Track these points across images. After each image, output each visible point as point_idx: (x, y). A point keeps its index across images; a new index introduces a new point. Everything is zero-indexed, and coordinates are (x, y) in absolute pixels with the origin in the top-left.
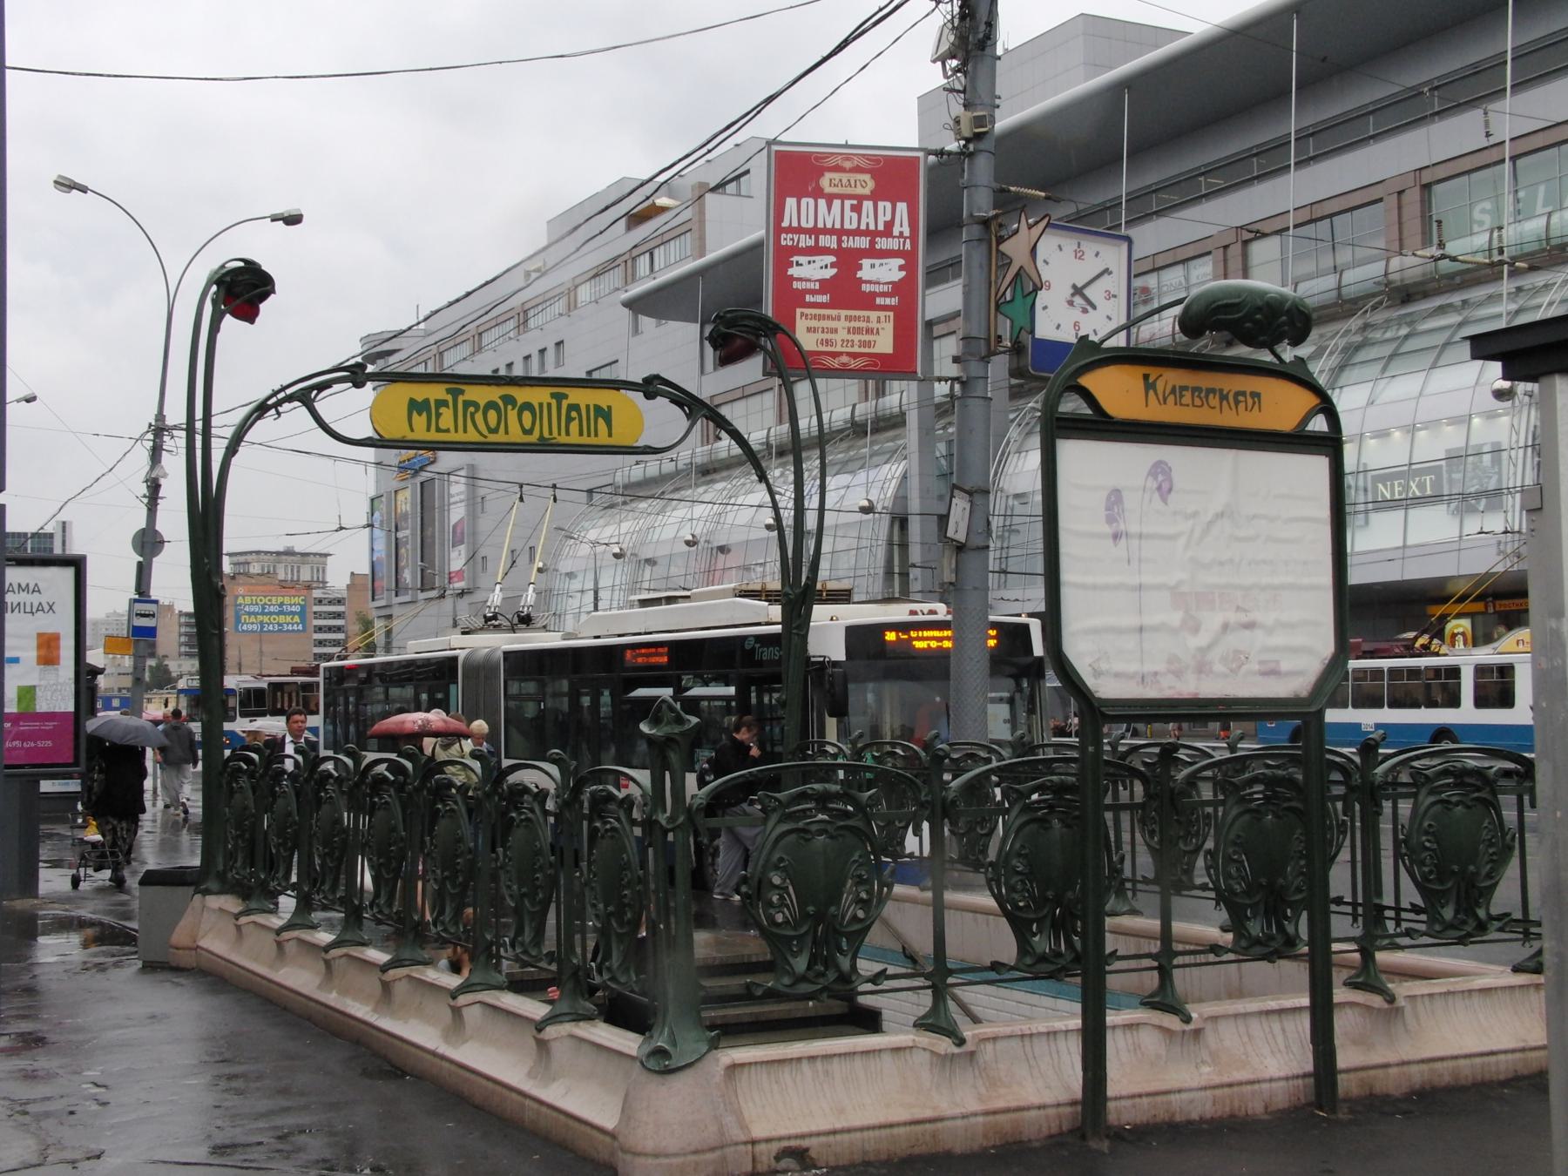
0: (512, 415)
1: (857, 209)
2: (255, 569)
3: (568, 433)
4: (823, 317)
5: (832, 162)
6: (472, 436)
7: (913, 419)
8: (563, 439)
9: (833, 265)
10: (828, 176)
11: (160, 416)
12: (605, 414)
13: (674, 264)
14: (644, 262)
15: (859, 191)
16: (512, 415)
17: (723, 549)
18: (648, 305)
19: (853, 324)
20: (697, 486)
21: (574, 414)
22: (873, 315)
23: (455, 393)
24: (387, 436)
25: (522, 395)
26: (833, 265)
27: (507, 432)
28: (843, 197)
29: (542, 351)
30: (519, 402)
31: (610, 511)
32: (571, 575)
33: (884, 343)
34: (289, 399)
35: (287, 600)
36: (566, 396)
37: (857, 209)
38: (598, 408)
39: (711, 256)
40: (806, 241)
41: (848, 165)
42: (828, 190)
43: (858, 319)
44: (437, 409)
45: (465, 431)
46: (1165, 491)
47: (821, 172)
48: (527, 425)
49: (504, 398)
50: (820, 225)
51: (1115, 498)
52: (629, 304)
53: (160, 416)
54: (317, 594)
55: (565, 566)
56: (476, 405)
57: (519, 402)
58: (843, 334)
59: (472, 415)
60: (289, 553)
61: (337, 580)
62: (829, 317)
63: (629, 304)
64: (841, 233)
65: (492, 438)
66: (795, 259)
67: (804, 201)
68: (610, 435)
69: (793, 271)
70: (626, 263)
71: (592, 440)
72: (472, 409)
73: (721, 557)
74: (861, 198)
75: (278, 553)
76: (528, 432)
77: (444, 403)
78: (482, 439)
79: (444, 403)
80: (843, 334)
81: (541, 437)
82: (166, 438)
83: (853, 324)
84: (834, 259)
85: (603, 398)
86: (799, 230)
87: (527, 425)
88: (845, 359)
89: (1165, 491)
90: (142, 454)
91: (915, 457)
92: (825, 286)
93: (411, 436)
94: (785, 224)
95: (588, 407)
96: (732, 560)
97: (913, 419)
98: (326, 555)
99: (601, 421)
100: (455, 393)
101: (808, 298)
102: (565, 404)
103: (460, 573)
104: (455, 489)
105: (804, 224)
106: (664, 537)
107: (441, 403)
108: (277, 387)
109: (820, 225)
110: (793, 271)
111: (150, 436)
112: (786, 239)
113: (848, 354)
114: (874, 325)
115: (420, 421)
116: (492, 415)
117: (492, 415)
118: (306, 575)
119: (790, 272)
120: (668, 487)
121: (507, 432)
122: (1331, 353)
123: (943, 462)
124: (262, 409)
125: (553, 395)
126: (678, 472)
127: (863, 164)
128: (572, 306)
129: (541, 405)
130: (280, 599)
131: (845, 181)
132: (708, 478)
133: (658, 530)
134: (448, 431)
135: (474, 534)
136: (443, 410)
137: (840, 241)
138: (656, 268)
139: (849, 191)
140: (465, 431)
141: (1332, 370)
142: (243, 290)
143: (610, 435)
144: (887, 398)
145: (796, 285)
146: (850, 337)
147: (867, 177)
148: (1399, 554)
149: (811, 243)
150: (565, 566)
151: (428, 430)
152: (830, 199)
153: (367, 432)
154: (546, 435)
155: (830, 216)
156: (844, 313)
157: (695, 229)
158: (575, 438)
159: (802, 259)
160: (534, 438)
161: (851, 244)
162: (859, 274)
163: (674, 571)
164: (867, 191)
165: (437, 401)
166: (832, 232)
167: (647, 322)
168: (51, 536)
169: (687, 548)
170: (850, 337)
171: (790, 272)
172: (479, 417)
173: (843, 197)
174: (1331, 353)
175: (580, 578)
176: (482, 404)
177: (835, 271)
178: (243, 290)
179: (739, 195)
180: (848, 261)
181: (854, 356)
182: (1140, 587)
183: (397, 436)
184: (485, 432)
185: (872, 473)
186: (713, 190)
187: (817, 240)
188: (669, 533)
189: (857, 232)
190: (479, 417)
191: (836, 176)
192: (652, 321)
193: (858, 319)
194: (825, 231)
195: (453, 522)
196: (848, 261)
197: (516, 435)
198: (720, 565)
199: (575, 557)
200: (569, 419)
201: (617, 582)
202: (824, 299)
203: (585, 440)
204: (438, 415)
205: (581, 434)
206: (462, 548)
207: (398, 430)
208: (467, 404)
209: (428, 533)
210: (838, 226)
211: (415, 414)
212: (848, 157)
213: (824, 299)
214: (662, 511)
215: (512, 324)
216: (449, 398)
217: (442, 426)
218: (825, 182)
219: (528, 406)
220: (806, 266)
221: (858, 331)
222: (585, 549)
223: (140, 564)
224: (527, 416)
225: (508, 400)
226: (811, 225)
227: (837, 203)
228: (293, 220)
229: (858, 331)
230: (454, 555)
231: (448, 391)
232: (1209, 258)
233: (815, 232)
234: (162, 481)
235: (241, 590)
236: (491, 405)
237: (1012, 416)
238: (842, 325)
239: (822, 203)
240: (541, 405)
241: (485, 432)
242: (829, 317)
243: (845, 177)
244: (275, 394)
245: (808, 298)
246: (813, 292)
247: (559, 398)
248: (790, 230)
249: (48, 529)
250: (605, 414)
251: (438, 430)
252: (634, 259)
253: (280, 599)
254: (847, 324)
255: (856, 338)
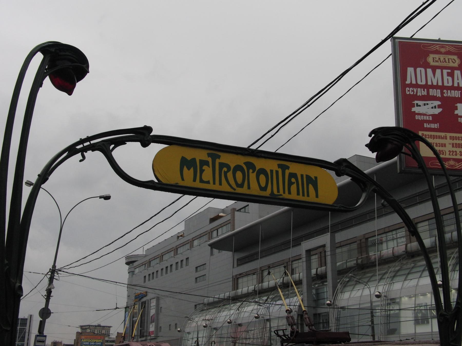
0: (253, 176)
1: (451, 75)
2: (88, 331)
4: (436, 137)
5: (433, 48)
6: (225, 188)
7: (305, 282)
8: (286, 196)
9: (439, 106)
10: (432, 56)
11: (54, 266)
12: (313, 182)
13: (224, 233)
14: (215, 233)
15: (451, 64)
16: (253, 176)
17: (240, 325)
18: (219, 245)
19: (455, 141)
20: (232, 304)
21: (293, 180)
23: (214, 157)
24: (164, 181)
25: (259, 163)
26: (439, 106)
27: (249, 188)
28: (442, 68)
29: (182, 261)
31: (202, 312)
32: (189, 333)
34: (93, 148)
35: (97, 341)
36: (288, 168)
37: (451, 75)
39: (236, 230)
40: (421, 92)
41: (443, 50)
42: (432, 64)
44: (201, 167)
47: (427, 54)
48: (263, 184)
49: (246, 163)
50: (430, 83)
52: (210, 245)
53: (54, 266)
54: (107, 339)
55: (187, 330)
58: (449, 148)
59: (226, 173)
60: (99, 326)
61: (113, 335)
62: (440, 137)
63: (210, 245)
64: (442, 88)
65: (239, 190)
66: (416, 102)
67: (418, 69)
68: (317, 196)
69: (415, 109)
70: (210, 234)
72: (225, 169)
73: (239, 328)
74: (453, 69)
75: (96, 326)
76: (264, 189)
78: (232, 191)
79: (207, 163)
80: (449, 148)
82: (55, 274)
83: (455, 141)
84: (439, 103)
85: (313, 171)
86: (417, 86)
88: (452, 163)
90: (46, 281)
91: (305, 294)
92: (435, 118)
93: (181, 183)
94: (408, 82)
95: (302, 176)
96: (243, 328)
97: (305, 282)
98: (110, 327)
99: (311, 186)
100: (214, 157)
101: (426, 125)
102: (287, 172)
103: (152, 332)
104: (152, 305)
105: (419, 82)
106: (220, 321)
107: (204, 163)
108: (84, 137)
109: (430, 83)
110: (415, 109)
111: (50, 273)
112: (409, 91)
113: (454, 160)
115: (188, 173)
116: (239, 175)
118: (104, 332)
119: (413, 109)
120: (221, 304)
121: (249, 188)
122: (453, 259)
123: (314, 296)
124: (71, 150)
126: (224, 299)
127: (452, 50)
128: (192, 246)
129: (272, 171)
130: (95, 340)
131: (442, 59)
132: (235, 301)
133: (218, 318)
134: (208, 182)
135: (158, 319)
136: (205, 167)
137: (442, 93)
138: (219, 235)
139: (445, 64)
140: (220, 184)
141: (454, 265)
142: (64, 65)
143: (317, 196)
144: (294, 276)
145: (417, 117)
146: (454, 149)
147: (455, 57)
148: (431, 334)
149: (425, 93)
150: (187, 330)
151: (195, 180)
152: (434, 69)
153: (150, 176)
154: (275, 192)
155: (435, 78)
156: (449, 135)
157: (231, 223)
159: (420, 103)
160: (267, 193)
161: (449, 94)
162: (456, 112)
163: (223, 332)
164: (456, 65)
165: (201, 161)
166: (436, 87)
167: (215, 251)
168: (27, 319)
169: (228, 324)
170: (454, 149)
171: (413, 109)
173: (442, 68)
174: (453, 259)
175: (192, 334)
176: (232, 166)
177: (440, 110)
178: (64, 65)
179: (245, 212)
180: (448, 105)
183: (173, 182)
184: (234, 186)
185: (291, 299)
186: (238, 211)
187: (428, 92)
188: (222, 320)
189: (452, 88)
190: (230, 175)
191: (437, 56)
192: (217, 251)
194: (433, 87)
195: (151, 315)
196: (448, 105)
197: (255, 190)
198: (239, 330)
199: (191, 326)
200: (290, 184)
201: (204, 335)
202: (436, 126)
204: (202, 171)
205: (298, 194)
206: (154, 324)
207: (175, 179)
208: (222, 165)
209: (143, 318)
210: (440, 84)
211: (185, 168)
212: (443, 47)
213: (436, 126)
214: (220, 312)
215: (172, 253)
216: (210, 160)
217: (205, 178)
218: (430, 59)
219: (262, 171)
220: (423, 107)
222: (194, 324)
223: (41, 321)
224: (262, 178)
225: (250, 166)
226: (424, 83)
227: (438, 72)
228: (107, 198)
230: (151, 326)
231: (209, 155)
232: (404, 229)
233: (426, 87)
234: (52, 290)
235: (83, 337)
236: (238, 168)
237: (338, 281)
238: (448, 142)
239: (429, 71)
240: (272, 171)
241: (234, 186)
242: (440, 137)
243: (442, 57)
244: (82, 141)
245: (426, 125)
246: (428, 122)
248: (411, 85)
249: (26, 317)
250: (313, 182)
251: (202, 181)
252: (212, 232)
253: (95, 340)
254: (452, 141)
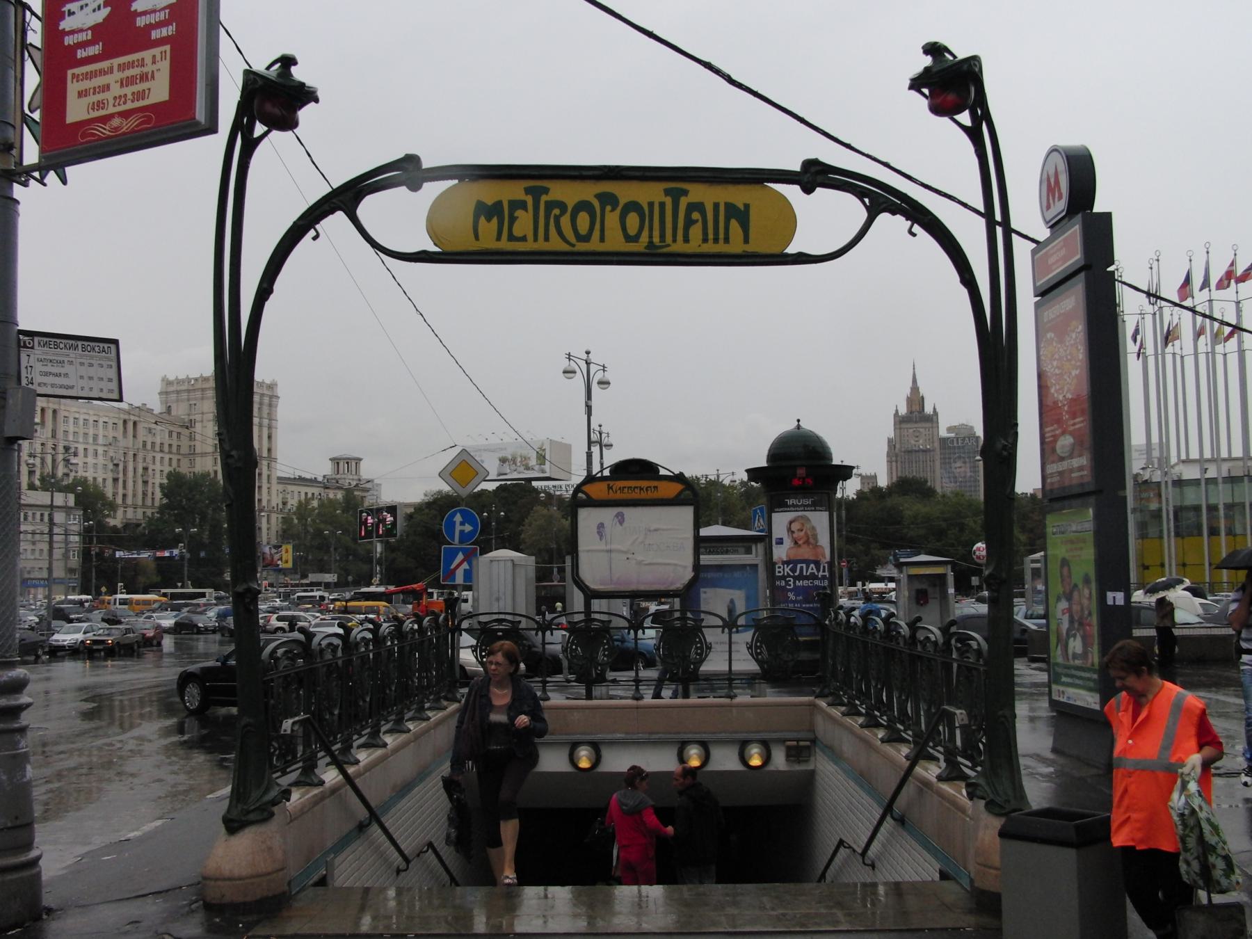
0: (612, 218)
3: (686, 240)
6: (556, 244)
12: (741, 215)
16: (612, 218)
21: (696, 215)
22: (147, 55)
23: (536, 193)
27: (602, 239)
30: (622, 201)
33: (159, 91)
38: (730, 207)
43: (131, 65)
45: (547, 239)
46: (621, 522)
51: (601, 526)
56: (562, 206)
57: (622, 201)
59: (557, 219)
65: (582, 247)
68: (746, 241)
71: (721, 248)
72: (557, 211)
77: (522, 205)
79: (522, 205)
81: (651, 243)
87: (632, 231)
88: (116, 122)
89: (621, 522)
92: (98, 31)
95: (716, 206)
99: (734, 224)
100: (536, 193)
102: (684, 202)
107: (517, 205)
114: (148, 68)
116: (583, 220)
117: (583, 220)
121: (602, 239)
125: (667, 192)
129: (651, 205)
134: (524, 239)
136: (519, 213)
140: (547, 239)
143: (746, 241)
151: (499, 238)
156: (116, 62)
158: (695, 245)
160: (640, 247)
172: (565, 221)
181: (125, 115)
182: (610, 551)
184: (572, 239)
190: (565, 221)
193: (131, 65)
197: (615, 241)
200: (689, 223)
203: (710, 248)
204: (513, 219)
208: (550, 205)
216: (529, 200)
217: (517, 231)
219: (633, 206)
221: (130, 81)
224: (633, 220)
225: (608, 200)
229: (130, 81)
236: (583, 206)
238: (112, 79)
240: (651, 205)
246: (84, 45)
247: (676, 195)
251: (512, 238)
255: (129, 91)
